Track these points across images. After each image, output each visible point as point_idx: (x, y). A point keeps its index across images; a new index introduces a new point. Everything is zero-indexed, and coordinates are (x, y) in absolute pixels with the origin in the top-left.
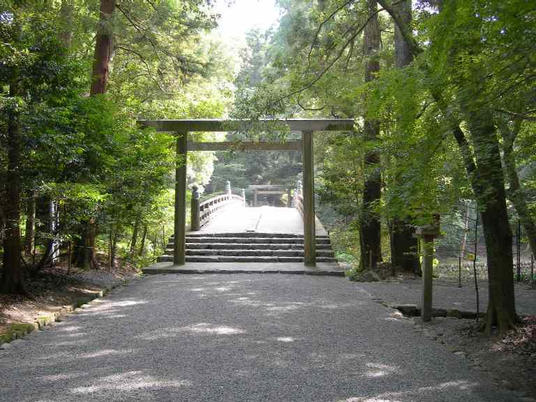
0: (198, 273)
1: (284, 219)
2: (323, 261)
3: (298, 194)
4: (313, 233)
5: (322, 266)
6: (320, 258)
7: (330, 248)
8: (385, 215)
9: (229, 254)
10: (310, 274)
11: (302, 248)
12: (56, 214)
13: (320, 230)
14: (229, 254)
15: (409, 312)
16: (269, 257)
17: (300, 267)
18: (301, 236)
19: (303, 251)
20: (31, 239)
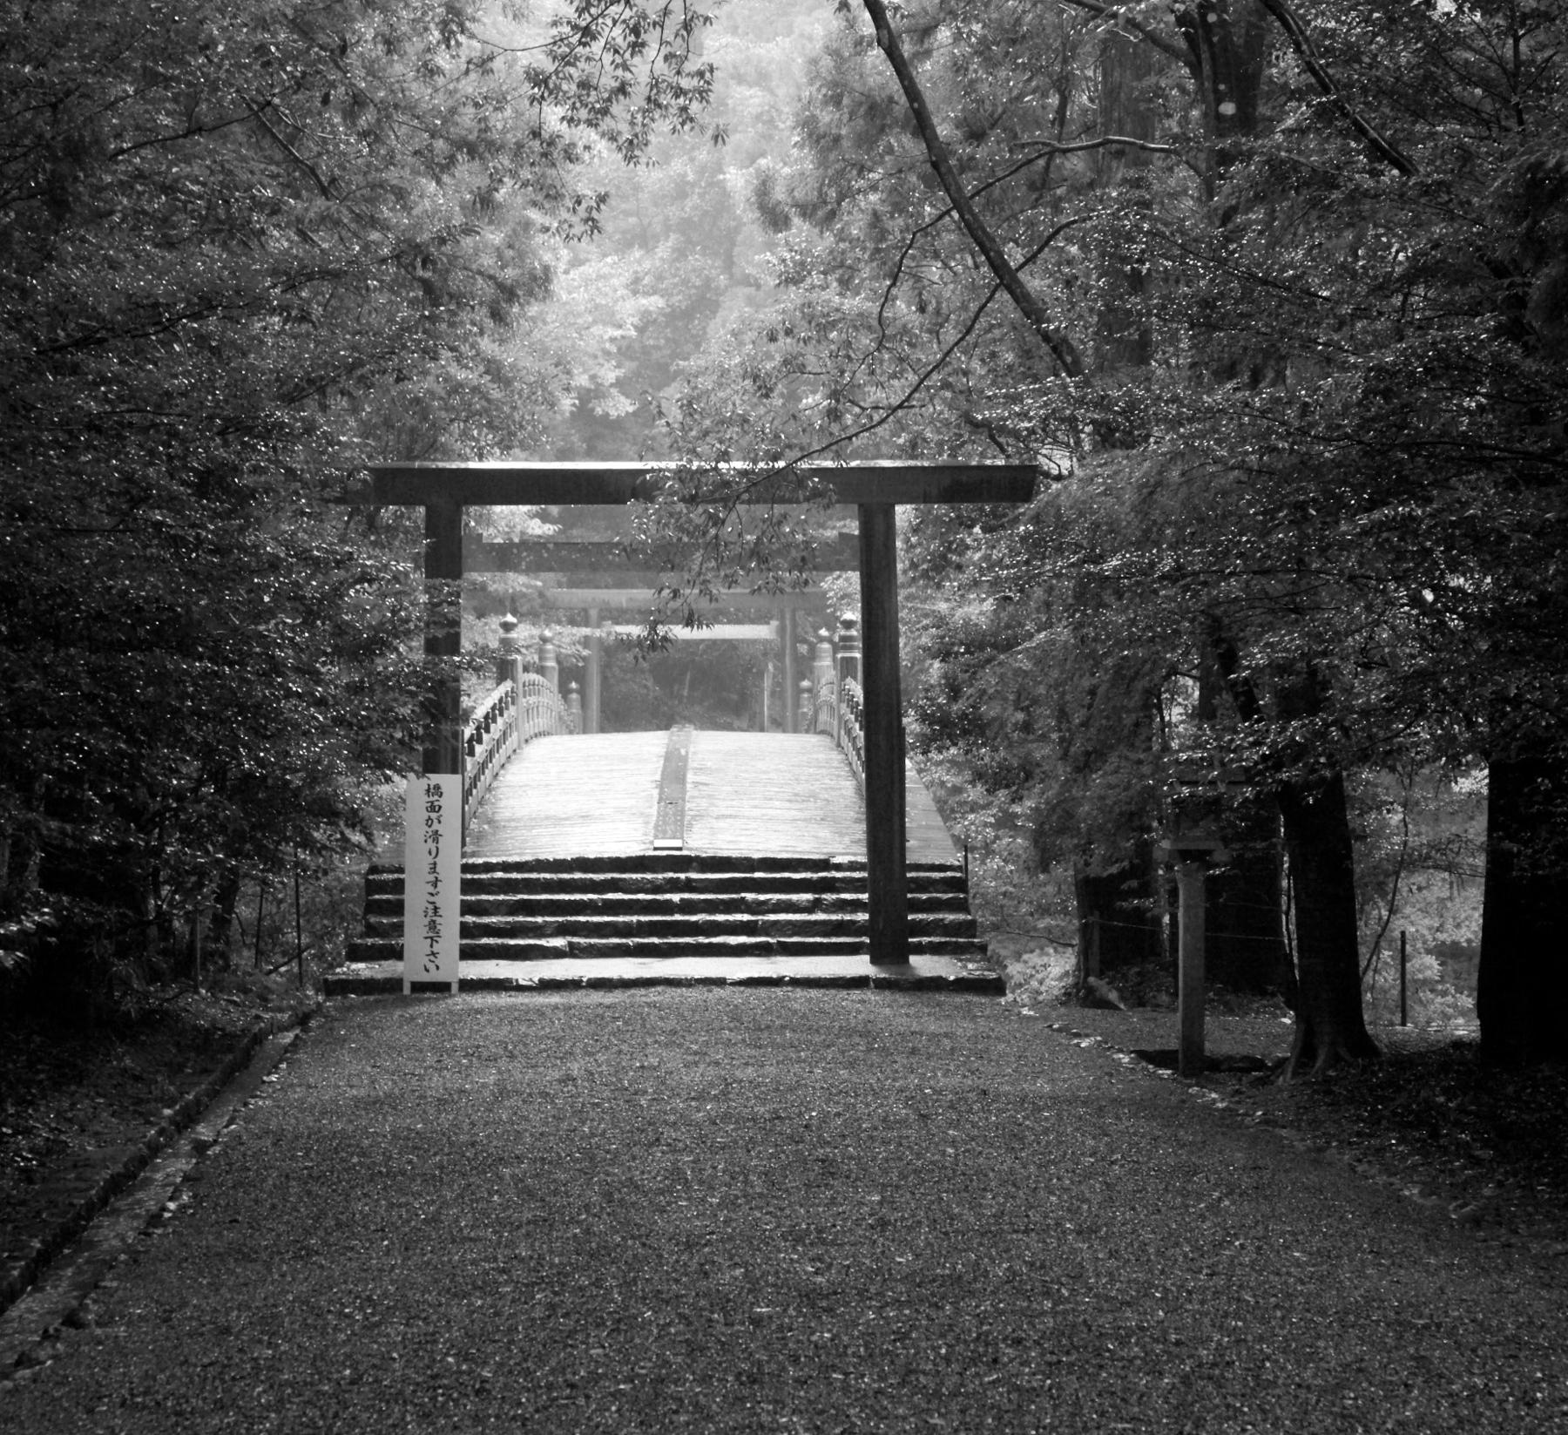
0: (520, 988)
1: (776, 793)
2: (935, 949)
3: (836, 684)
4: (897, 855)
5: (924, 965)
7: (962, 906)
8: (968, 775)
10: (881, 985)
11: (856, 906)
12: (1251, 849)
13: (928, 840)
16: (743, 939)
17: (859, 965)
18: (853, 866)
19: (862, 917)
20: (1402, 503)
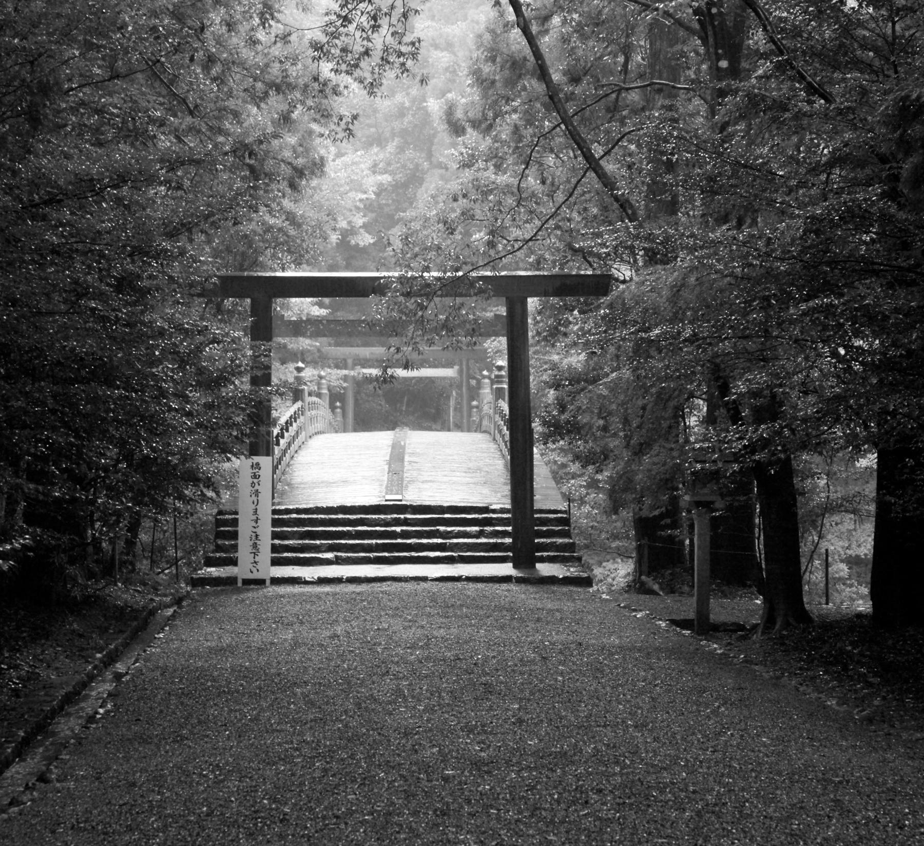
0: (307, 583)
1: (457, 468)
2: (551, 560)
3: (492, 403)
4: (528, 504)
5: (545, 569)
6: (545, 554)
7: (567, 534)
8: (570, 457)
9: (353, 548)
10: (519, 580)
11: (504, 534)
13: (547, 495)
14: (353, 548)
15: (684, 624)
16: (438, 554)
17: (506, 569)
18: (502, 511)
19: (508, 540)
